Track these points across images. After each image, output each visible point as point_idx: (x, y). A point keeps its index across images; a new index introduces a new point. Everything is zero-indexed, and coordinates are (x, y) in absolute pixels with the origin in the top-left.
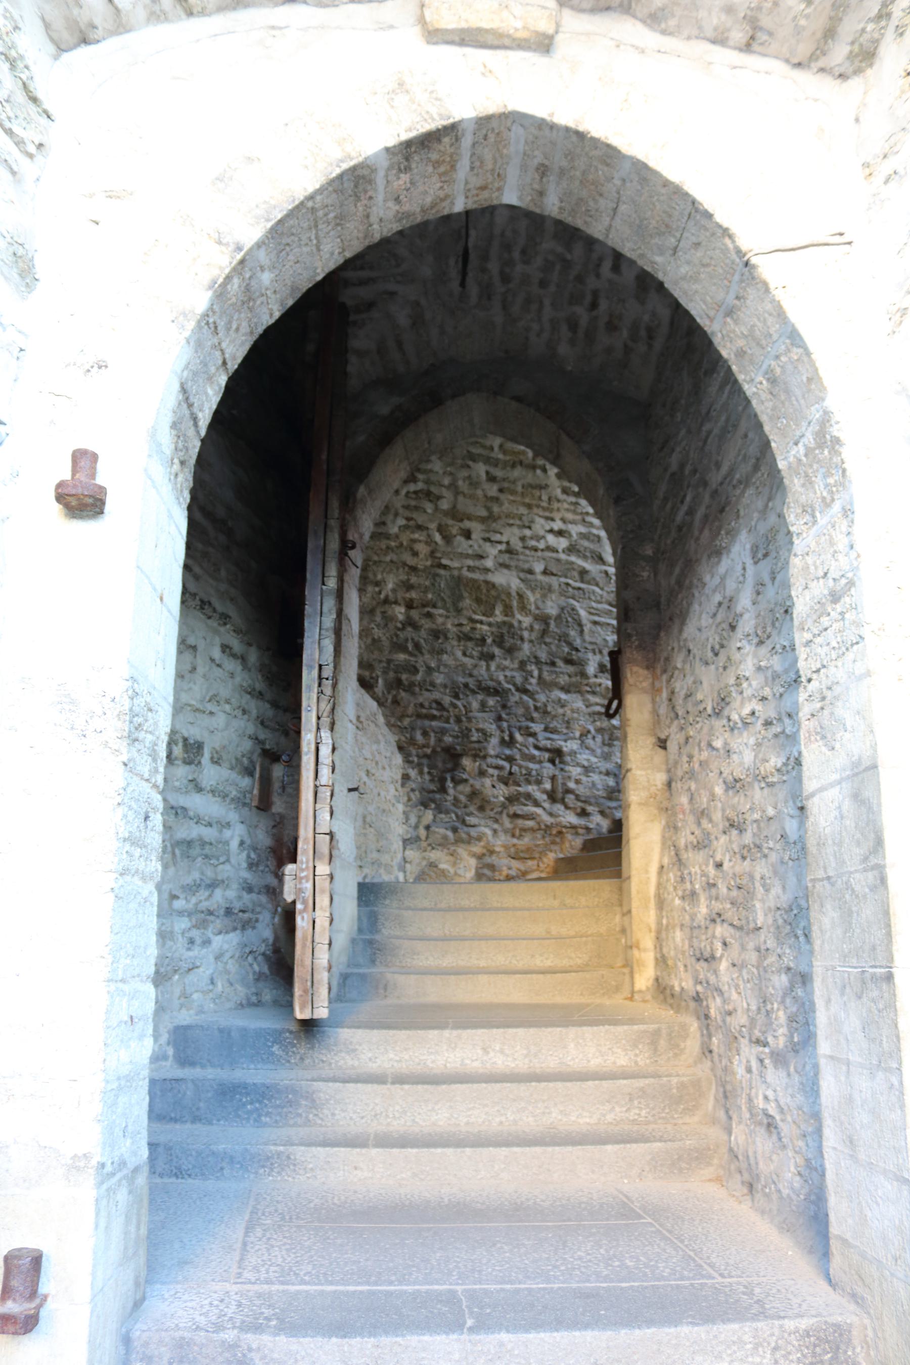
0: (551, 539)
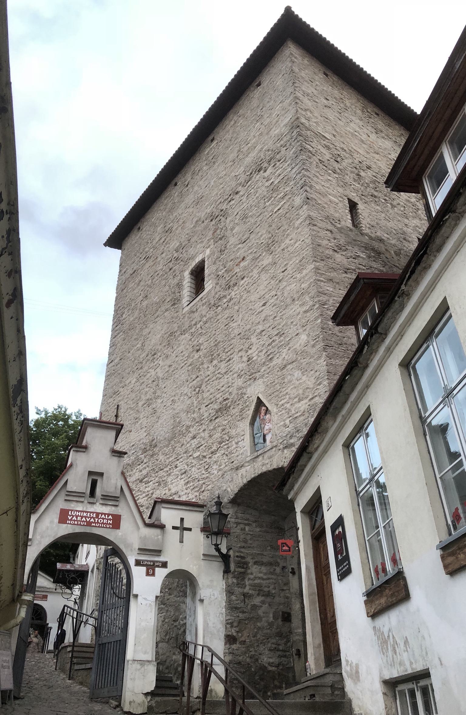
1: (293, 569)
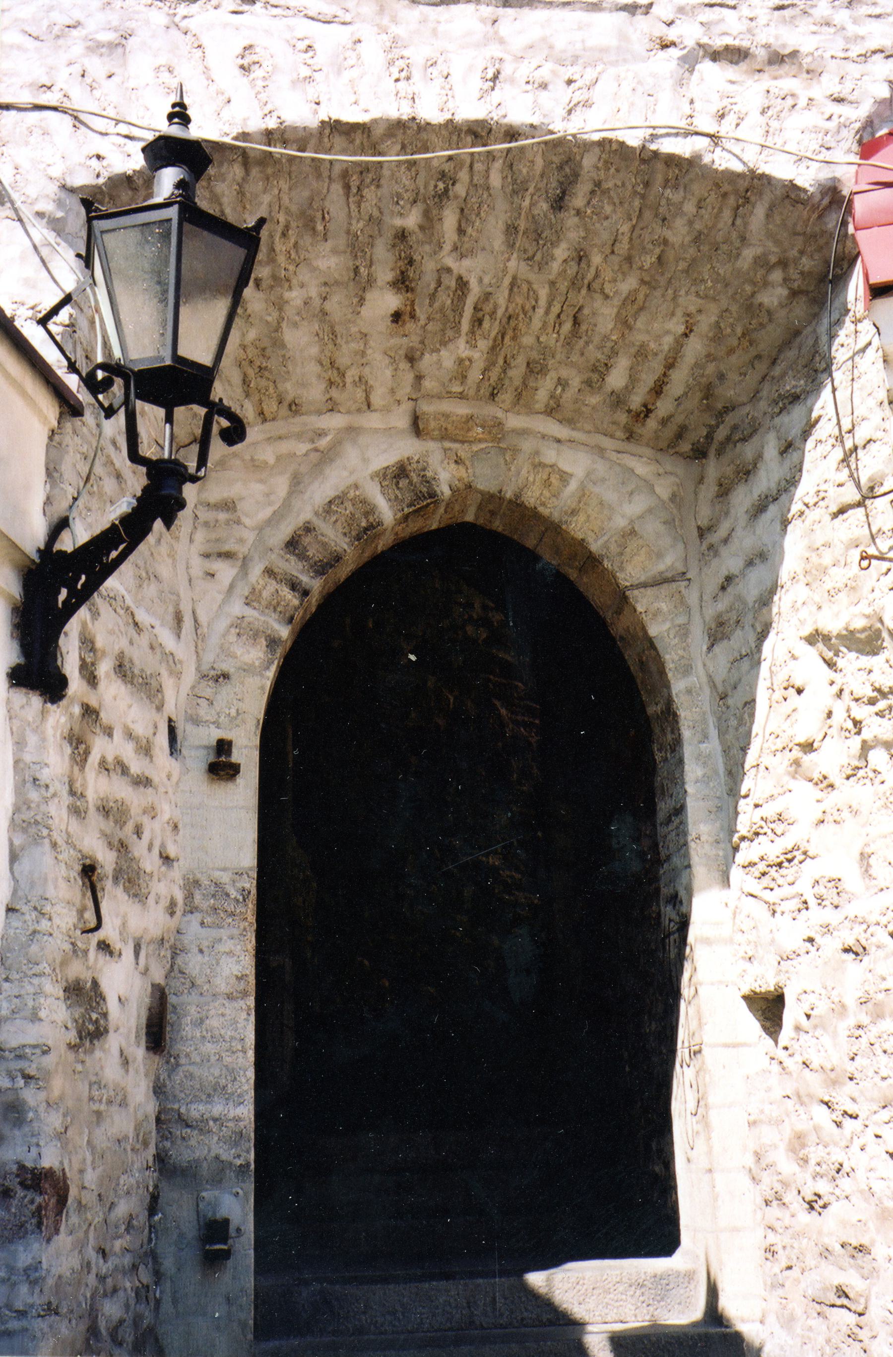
0: (469, 629)
1: (223, 747)
